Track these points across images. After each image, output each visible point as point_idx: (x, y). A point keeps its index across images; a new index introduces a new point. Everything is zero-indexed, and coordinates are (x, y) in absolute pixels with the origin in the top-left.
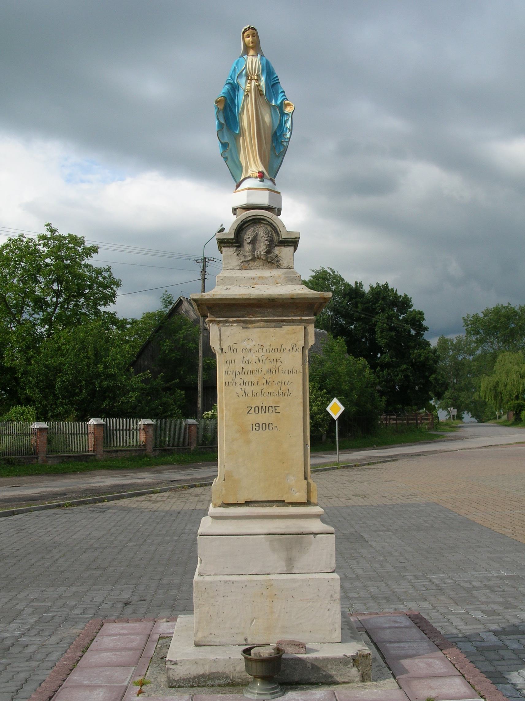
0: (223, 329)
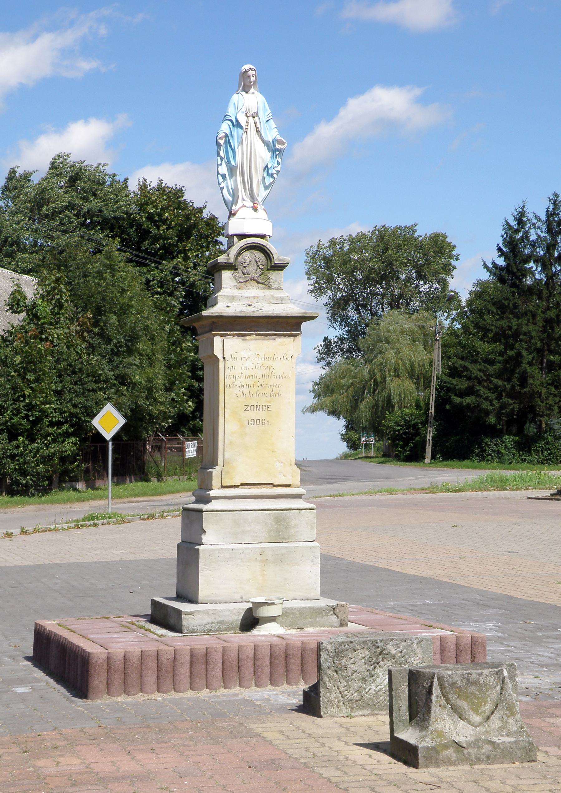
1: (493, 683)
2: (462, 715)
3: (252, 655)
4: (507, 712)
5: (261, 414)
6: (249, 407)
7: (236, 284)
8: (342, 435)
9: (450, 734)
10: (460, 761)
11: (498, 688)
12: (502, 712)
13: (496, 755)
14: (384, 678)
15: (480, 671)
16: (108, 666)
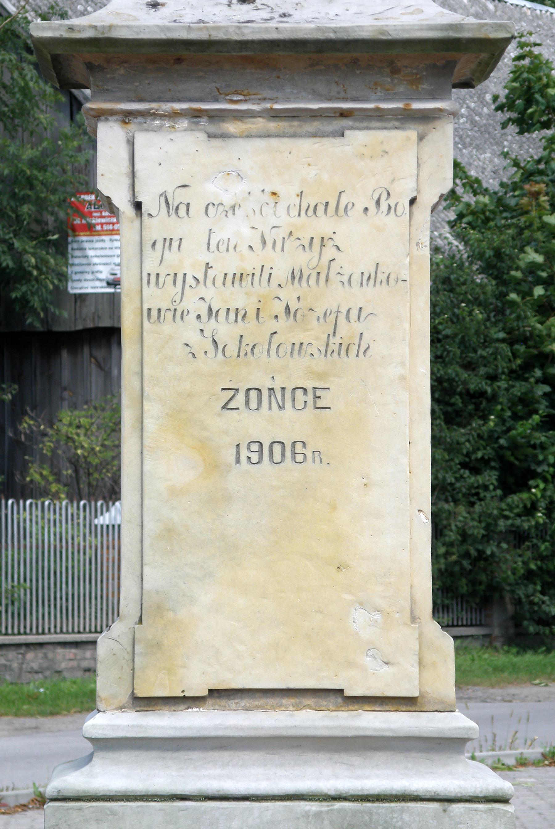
0: (141, 139)
6: (241, 398)
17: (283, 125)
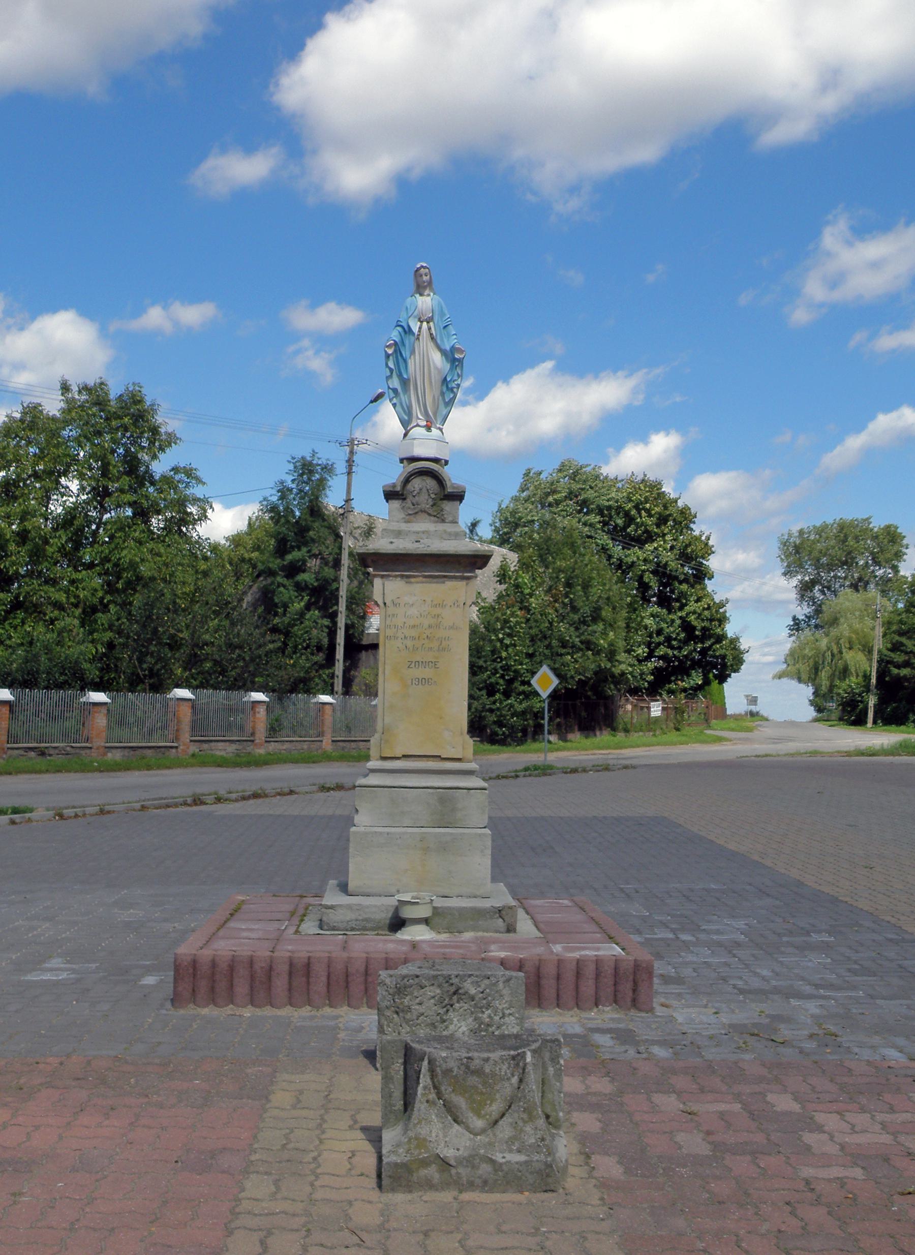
0: (386, 583)
1: (506, 1072)
2: (458, 1117)
3: (362, 969)
4: (525, 1116)
5: (427, 673)
6: (413, 664)
7: (404, 516)
8: (810, 701)
9: (436, 1144)
10: (445, 1185)
11: (515, 1080)
12: (516, 1115)
13: (497, 1180)
14: (459, 1025)
15: (486, 1055)
16: (194, 970)
17: (428, 580)
